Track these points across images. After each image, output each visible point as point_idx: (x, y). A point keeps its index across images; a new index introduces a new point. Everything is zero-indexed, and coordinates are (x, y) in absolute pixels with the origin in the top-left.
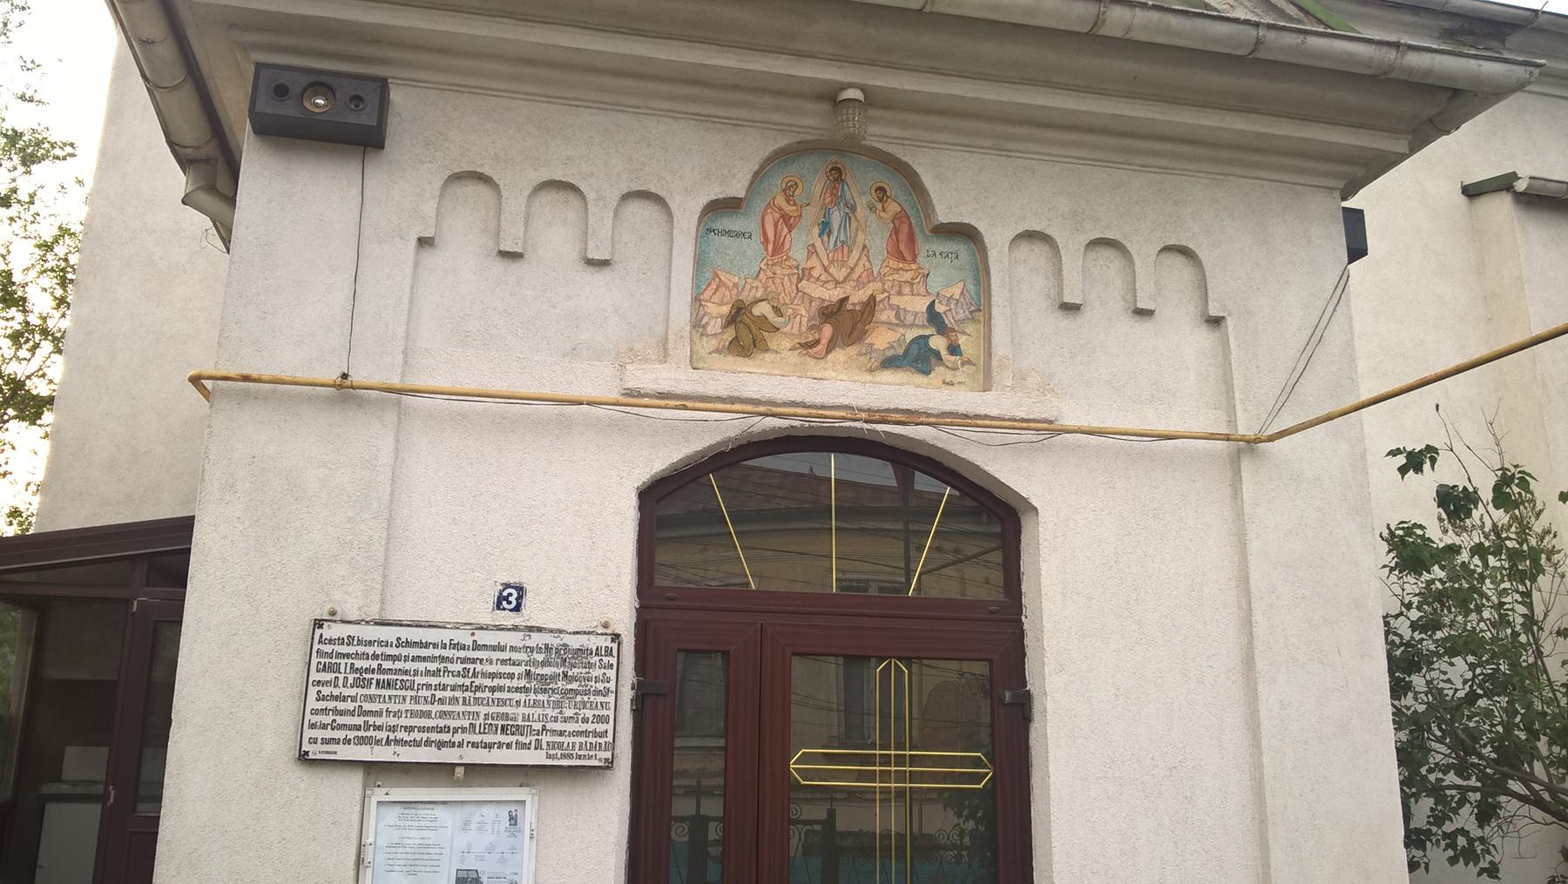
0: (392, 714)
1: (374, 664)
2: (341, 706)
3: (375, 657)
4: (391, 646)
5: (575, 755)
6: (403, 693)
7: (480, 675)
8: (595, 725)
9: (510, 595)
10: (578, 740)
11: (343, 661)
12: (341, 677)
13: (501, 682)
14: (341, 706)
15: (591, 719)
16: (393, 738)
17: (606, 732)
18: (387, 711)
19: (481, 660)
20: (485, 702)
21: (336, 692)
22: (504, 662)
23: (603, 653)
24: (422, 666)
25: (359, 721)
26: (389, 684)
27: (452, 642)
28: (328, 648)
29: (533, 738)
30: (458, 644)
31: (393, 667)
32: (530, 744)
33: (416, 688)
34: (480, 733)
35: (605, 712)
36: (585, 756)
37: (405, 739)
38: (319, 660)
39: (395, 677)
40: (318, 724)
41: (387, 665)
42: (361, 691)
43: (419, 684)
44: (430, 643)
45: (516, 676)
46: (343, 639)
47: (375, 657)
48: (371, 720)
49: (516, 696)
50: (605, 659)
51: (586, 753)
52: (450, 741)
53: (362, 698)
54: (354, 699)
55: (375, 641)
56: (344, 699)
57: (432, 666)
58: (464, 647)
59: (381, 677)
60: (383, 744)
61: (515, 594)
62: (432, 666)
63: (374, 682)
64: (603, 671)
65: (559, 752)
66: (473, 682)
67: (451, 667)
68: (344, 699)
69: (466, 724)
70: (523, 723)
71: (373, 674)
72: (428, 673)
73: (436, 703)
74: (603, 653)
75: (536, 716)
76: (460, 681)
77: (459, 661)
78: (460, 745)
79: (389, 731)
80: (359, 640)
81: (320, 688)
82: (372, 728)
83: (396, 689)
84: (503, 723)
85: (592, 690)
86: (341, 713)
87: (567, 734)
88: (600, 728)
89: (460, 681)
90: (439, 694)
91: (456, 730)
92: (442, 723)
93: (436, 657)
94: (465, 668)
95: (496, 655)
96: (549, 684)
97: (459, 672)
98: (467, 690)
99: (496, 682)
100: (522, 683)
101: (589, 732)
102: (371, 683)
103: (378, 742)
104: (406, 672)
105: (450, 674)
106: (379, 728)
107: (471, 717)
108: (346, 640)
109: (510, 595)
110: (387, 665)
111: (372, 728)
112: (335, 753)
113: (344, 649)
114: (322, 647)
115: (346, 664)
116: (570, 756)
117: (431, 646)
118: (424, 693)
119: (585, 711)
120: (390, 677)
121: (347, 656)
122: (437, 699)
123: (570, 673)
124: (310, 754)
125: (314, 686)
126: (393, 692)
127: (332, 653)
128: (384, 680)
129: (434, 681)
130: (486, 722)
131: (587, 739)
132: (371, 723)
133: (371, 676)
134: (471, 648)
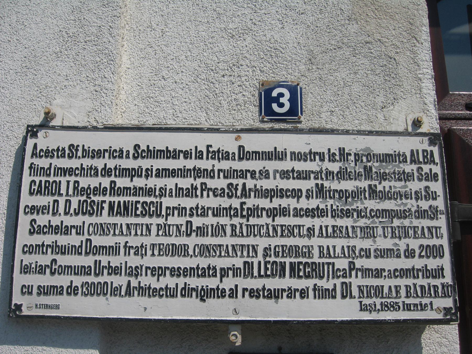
0: (132, 251)
1: (106, 182)
2: (63, 240)
3: (107, 172)
4: (128, 157)
5: (401, 304)
6: (146, 220)
7: (252, 194)
8: (424, 261)
9: (281, 95)
10: (403, 282)
11: (64, 180)
12: (62, 201)
13: (284, 202)
14: (63, 240)
15: (417, 252)
16: (137, 285)
17: (442, 269)
18: (125, 246)
19: (253, 174)
20: (263, 231)
21: (56, 221)
22: (285, 175)
23: (421, 159)
24: (170, 183)
25: (88, 261)
26: (126, 208)
27: (211, 149)
28: (43, 163)
29: (338, 282)
30: (219, 151)
31: (131, 185)
32: (334, 289)
33: (164, 213)
34: (260, 276)
35: (435, 242)
36: (415, 305)
37: (152, 287)
38: (32, 178)
39: (135, 199)
40: (33, 266)
41: (122, 182)
42: (88, 220)
43: (168, 208)
44: (180, 151)
45: (304, 194)
46: (64, 149)
47: (107, 172)
48: (104, 260)
49: (307, 222)
50: (426, 168)
51: (417, 301)
52: (218, 288)
53: (91, 229)
54: (79, 231)
55: (105, 151)
56: (66, 231)
57: (185, 183)
58: (226, 156)
59: (116, 199)
60: (123, 293)
61: (287, 95)
62: (185, 183)
63: (106, 206)
64: (424, 184)
65: (378, 301)
66: (244, 203)
67: (211, 183)
68: (66, 231)
69: (239, 262)
70: (321, 261)
71: (105, 195)
72: (180, 192)
73: (194, 234)
74: (421, 159)
75: (338, 250)
76: (225, 202)
77: (222, 174)
78: (233, 293)
79: (130, 275)
80: (84, 150)
81: (35, 216)
82: (106, 271)
83: (136, 215)
84: (293, 260)
85: (413, 210)
86: (63, 250)
87: (386, 274)
88: (433, 264)
89: (225, 202)
90: (197, 222)
91: (224, 273)
92: (204, 262)
93: (189, 170)
94: (231, 184)
95: (272, 165)
96: (352, 204)
97: (223, 189)
98: (236, 215)
99: (277, 202)
100: (314, 203)
101: (418, 270)
102: (102, 208)
103: (116, 291)
104: (150, 192)
105: (211, 193)
106: (115, 271)
107: (245, 253)
108: (67, 152)
109: (281, 95)
110: (122, 182)
111: (106, 271)
112: (57, 307)
113: (65, 163)
114: (36, 161)
115: (68, 182)
116: (394, 307)
117: (182, 155)
118: (174, 220)
119: (407, 241)
120: (127, 199)
121: (69, 171)
122: (194, 228)
123: (380, 188)
124: (23, 308)
125: (26, 213)
126: (132, 220)
127: (50, 168)
128: (119, 202)
129: (188, 203)
130: (268, 259)
131: (415, 281)
132: (104, 263)
133: (101, 198)
134: (237, 157)
